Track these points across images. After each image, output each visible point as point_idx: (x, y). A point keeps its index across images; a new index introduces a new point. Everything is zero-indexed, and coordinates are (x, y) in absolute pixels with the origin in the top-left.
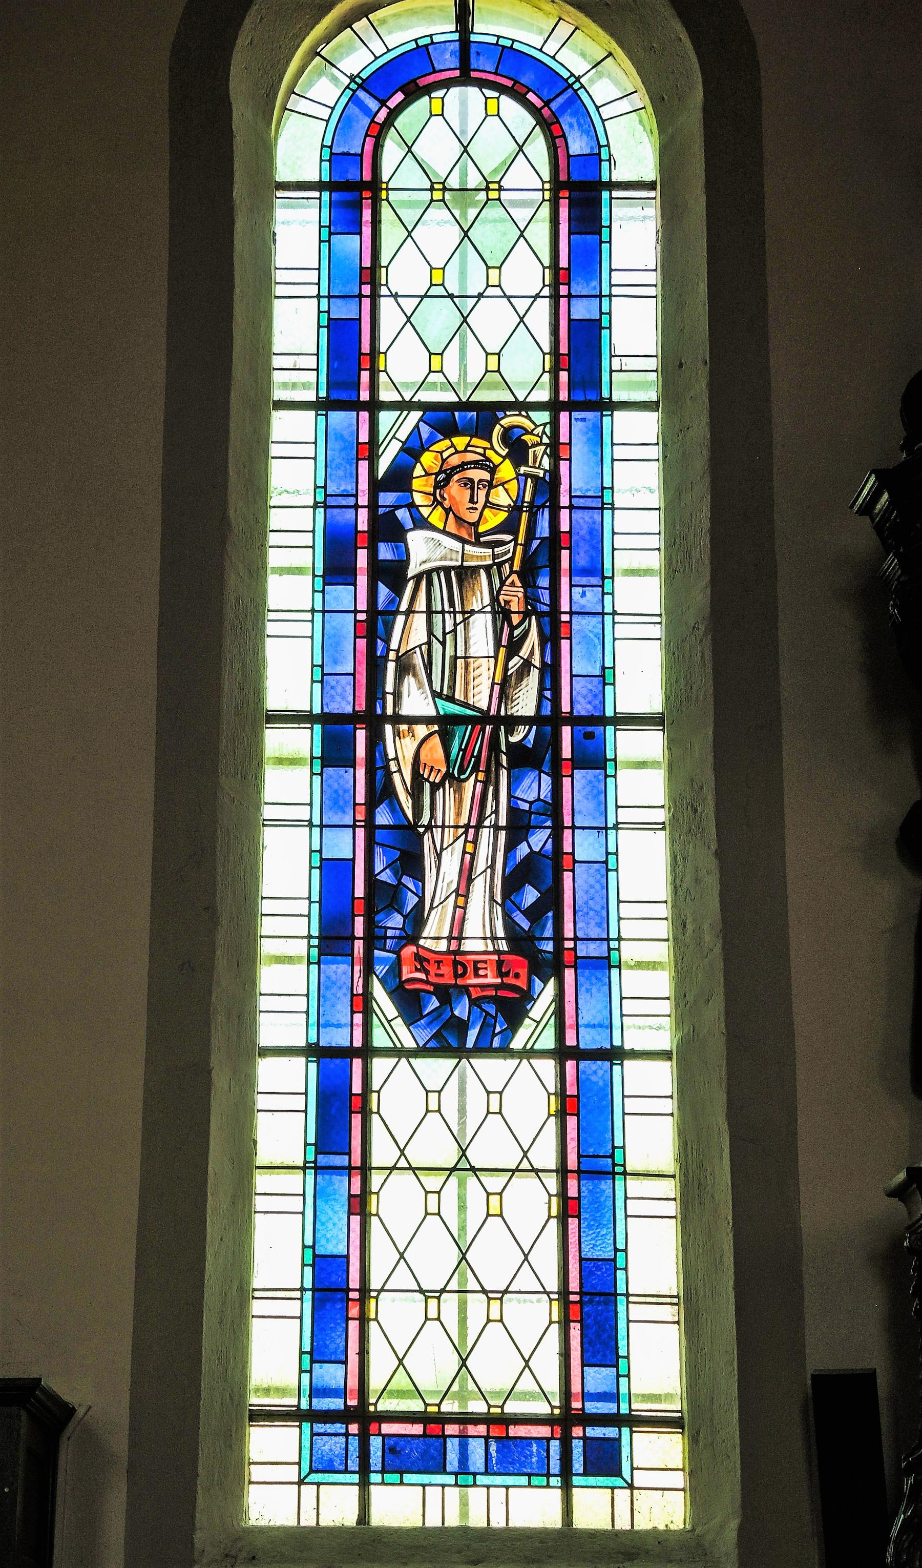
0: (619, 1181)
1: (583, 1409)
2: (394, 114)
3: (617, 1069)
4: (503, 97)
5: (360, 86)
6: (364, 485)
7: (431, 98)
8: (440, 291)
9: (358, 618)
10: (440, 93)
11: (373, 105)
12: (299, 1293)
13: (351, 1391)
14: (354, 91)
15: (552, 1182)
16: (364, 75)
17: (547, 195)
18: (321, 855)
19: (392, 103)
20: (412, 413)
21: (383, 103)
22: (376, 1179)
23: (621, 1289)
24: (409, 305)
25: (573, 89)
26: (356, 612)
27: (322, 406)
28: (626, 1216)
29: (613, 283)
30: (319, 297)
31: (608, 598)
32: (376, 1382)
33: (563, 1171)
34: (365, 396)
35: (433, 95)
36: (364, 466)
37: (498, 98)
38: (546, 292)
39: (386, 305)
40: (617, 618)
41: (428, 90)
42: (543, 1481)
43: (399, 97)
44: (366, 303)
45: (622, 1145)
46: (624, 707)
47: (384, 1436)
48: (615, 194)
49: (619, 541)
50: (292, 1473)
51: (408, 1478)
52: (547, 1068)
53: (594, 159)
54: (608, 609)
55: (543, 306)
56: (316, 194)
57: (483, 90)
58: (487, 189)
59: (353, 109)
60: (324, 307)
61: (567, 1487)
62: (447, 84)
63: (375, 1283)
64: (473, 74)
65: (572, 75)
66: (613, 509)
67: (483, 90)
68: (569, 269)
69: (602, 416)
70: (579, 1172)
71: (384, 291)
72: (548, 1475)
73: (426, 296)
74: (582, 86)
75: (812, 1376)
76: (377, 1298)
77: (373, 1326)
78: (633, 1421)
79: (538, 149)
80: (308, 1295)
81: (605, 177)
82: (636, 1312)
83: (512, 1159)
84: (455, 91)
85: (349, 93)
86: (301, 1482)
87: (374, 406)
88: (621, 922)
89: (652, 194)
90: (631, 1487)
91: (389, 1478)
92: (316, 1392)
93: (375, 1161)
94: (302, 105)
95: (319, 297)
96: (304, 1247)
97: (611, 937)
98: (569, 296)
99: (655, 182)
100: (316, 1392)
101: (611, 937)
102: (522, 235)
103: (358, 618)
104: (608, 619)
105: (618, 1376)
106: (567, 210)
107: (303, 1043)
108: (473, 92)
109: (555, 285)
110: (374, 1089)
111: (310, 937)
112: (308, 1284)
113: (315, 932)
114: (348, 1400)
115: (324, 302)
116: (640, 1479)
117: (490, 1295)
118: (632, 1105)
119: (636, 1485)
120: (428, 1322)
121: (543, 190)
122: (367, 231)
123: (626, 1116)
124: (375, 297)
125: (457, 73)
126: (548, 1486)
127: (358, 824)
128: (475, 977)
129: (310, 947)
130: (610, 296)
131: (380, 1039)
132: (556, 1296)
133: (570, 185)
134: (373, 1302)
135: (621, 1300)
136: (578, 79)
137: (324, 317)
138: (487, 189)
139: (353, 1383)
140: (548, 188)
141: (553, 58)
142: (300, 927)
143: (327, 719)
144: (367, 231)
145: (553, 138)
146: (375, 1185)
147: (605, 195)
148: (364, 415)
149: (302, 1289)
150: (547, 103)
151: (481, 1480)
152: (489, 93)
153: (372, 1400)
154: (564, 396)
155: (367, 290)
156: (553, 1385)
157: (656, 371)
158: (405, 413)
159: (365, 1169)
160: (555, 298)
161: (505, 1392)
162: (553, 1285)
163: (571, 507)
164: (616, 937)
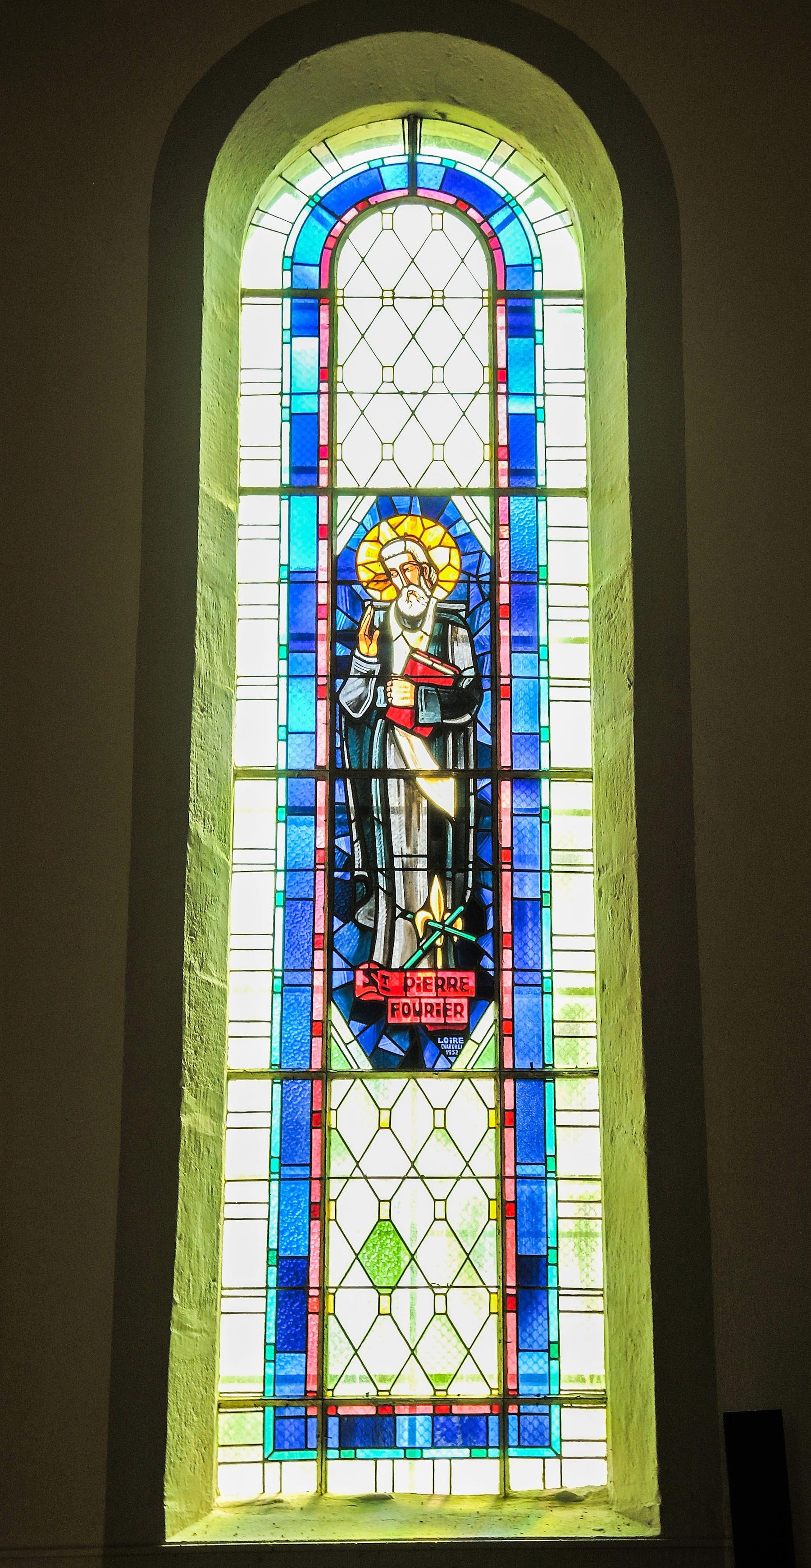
0: (551, 1184)
1: (517, 1390)
2: (348, 226)
3: (541, 505)
4: (446, 214)
5: (319, 204)
6: (324, 562)
7: (382, 213)
8: (390, 388)
9: (319, 683)
10: (392, 209)
11: (331, 220)
12: (264, 1291)
13: (320, 808)
14: (313, 208)
15: (491, 1187)
16: (322, 193)
17: (486, 302)
18: (292, 259)
19: (347, 217)
20: (367, 497)
21: (339, 218)
22: (334, 1187)
23: (552, 1283)
24: (362, 400)
25: (510, 207)
26: (316, 676)
27: (288, 491)
28: (552, 950)
29: (554, 948)
30: (282, 394)
31: (543, 664)
32: (333, 1368)
33: (501, 1178)
34: (323, 481)
35: (383, 211)
36: (323, 544)
37: (442, 214)
38: (486, 388)
39: (342, 400)
40: (561, 1292)
41: (381, 206)
42: (482, 1452)
43: (353, 213)
44: (324, 399)
45: (555, 1262)
46: (558, 763)
47: (341, 1417)
48: (547, 301)
49: (554, 613)
50: (257, 1453)
51: (361, 1453)
52: (488, 1087)
53: (528, 269)
54: (544, 673)
55: (484, 401)
56: (278, 300)
57: (430, 208)
58: (432, 297)
59: (313, 222)
60: (286, 403)
61: (504, 1458)
62: (395, 202)
63: (333, 1280)
64: (420, 193)
65: (508, 194)
66: (547, 584)
67: (430, 208)
68: (514, 1110)
69: (537, 501)
70: (516, 1177)
71: (340, 388)
72: (487, 1447)
73: (377, 393)
74: (518, 204)
75: (725, 1414)
76: (334, 1294)
77: (331, 1320)
78: (561, 1402)
79: (478, 256)
80: (273, 1293)
81: (537, 287)
82: (566, 1303)
83: (456, 1167)
84: (403, 208)
85: (308, 210)
86: (266, 1460)
87: (332, 493)
88: (549, 608)
89: (580, 302)
90: (559, 1456)
91: (346, 1453)
92: (278, 1380)
93: (333, 1172)
94: (266, 221)
95: (282, 394)
96: (269, 1250)
97: (543, 869)
98: (508, 394)
99: (587, 489)
100: (278, 1380)
101: (543, 869)
102: (463, 338)
103: (319, 683)
104: (543, 683)
105: (535, 344)
106: (504, 317)
107: (278, 485)
108: (421, 210)
109: (494, 383)
110: (339, 363)
111: (273, 970)
112: (273, 1283)
113: (279, 965)
114: (314, 820)
115: (286, 399)
116: (568, 1449)
117: (437, 1291)
118: (552, 454)
119: (563, 1455)
120: (380, 1130)
121: (483, 298)
122: (325, 333)
123: (551, 688)
124: (332, 394)
125: (406, 192)
126: (487, 1457)
127: (318, 867)
128: (424, 991)
129: (274, 977)
130: (544, 395)
131: (484, 503)
132: (495, 1290)
133: (506, 295)
134: (331, 1297)
135: (553, 1294)
136: (514, 199)
137: (286, 412)
138: (432, 297)
139: (313, 1371)
140: (487, 296)
141: (492, 178)
142: (264, 960)
143: (293, 774)
144: (325, 333)
145: (491, 251)
146: (333, 1193)
147: (538, 302)
148: (324, 501)
149: (267, 1288)
150: (486, 219)
151: (427, 1453)
152: (434, 210)
153: (330, 1386)
154: (503, 482)
155: (324, 387)
156: (493, 1371)
157: (584, 382)
158: (360, 497)
159: (323, 1179)
160: (494, 394)
161: (450, 1375)
162: (492, 1279)
163: (514, 970)
164: (542, 393)
